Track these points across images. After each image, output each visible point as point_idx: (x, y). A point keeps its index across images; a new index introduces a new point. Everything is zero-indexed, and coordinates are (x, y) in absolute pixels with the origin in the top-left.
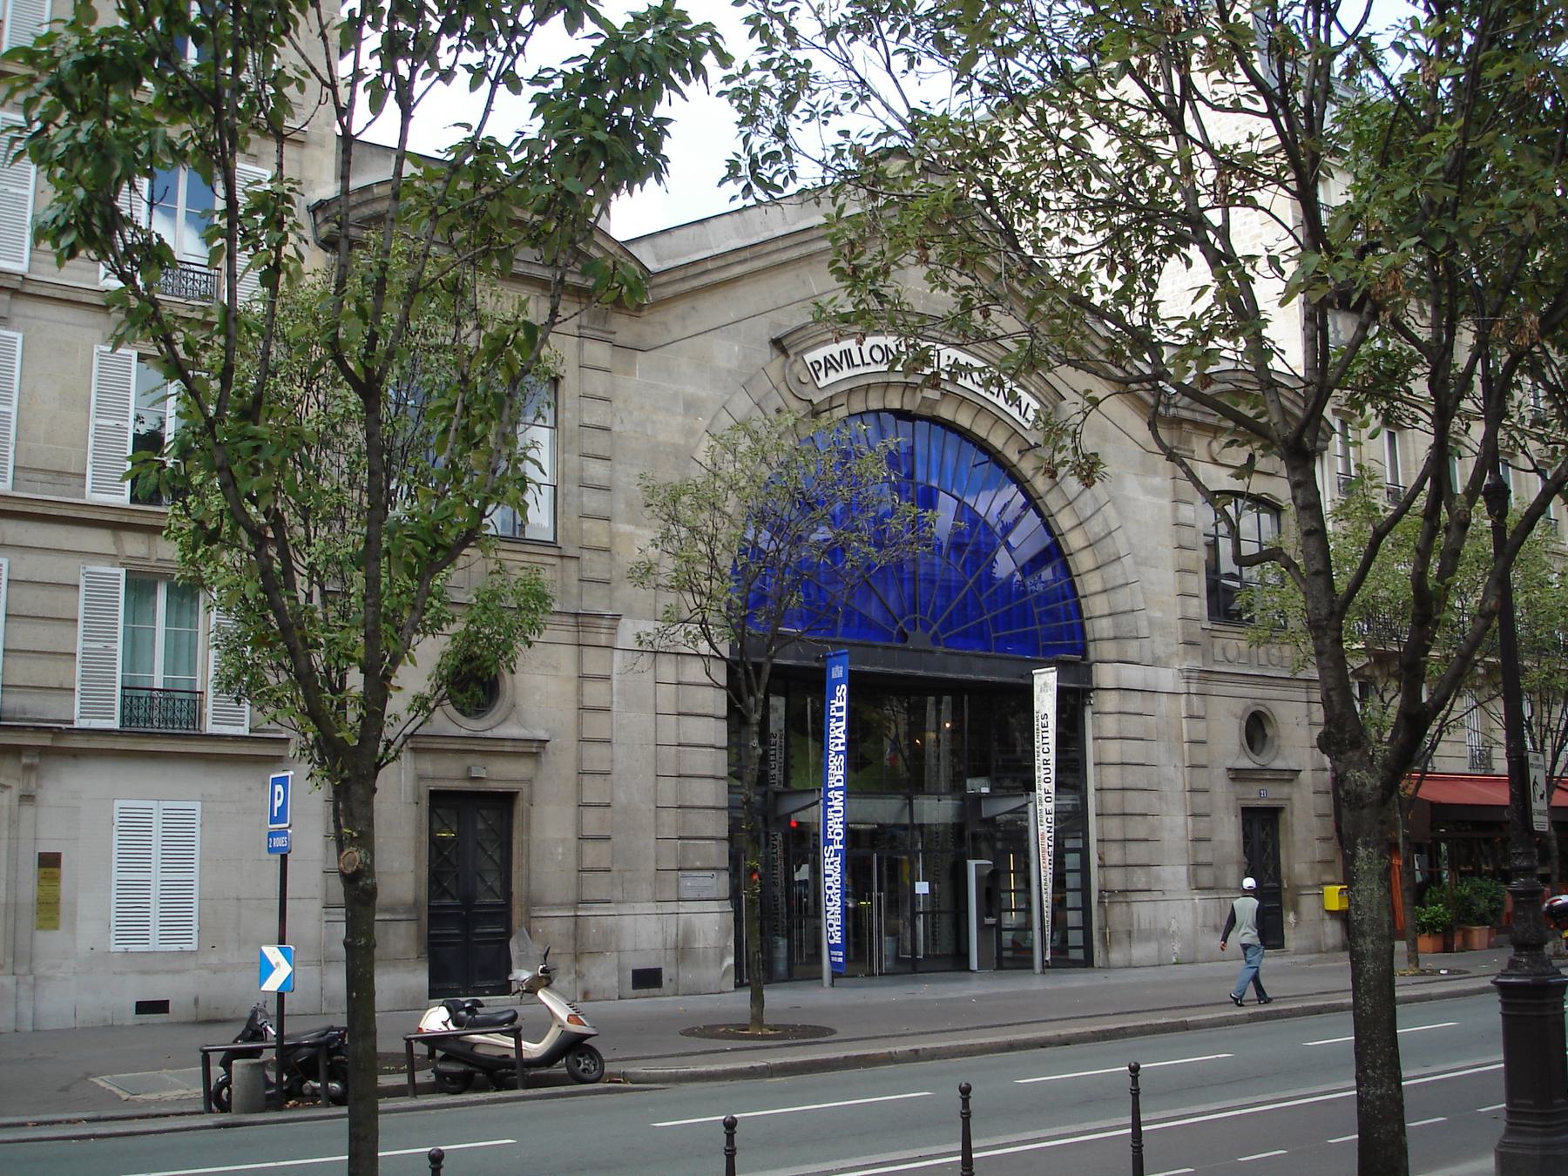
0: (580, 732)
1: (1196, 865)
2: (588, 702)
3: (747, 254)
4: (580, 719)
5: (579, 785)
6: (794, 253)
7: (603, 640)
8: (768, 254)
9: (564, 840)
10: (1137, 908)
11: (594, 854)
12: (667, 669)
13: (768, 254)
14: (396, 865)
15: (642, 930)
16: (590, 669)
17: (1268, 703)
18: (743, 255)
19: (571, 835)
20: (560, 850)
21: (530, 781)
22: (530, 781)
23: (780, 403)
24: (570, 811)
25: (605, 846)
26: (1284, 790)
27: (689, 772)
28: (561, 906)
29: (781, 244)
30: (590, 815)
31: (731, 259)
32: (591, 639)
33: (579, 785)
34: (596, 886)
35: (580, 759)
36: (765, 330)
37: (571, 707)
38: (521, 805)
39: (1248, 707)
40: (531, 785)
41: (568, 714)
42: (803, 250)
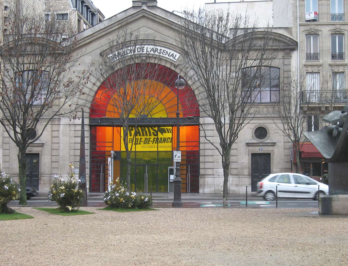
0: (52, 142)
1: (58, 131)
2: (53, 136)
3: (90, 37)
4: (52, 139)
5: (52, 152)
6: (103, 33)
7: (57, 123)
8: (96, 35)
9: (48, 162)
10: (206, 179)
11: (54, 165)
12: (73, 128)
13: (96, 35)
14: (16, 167)
15: (76, 190)
16: (54, 129)
17: (265, 125)
18: (89, 37)
19: (50, 161)
20: (48, 164)
21: (41, 151)
22: (41, 151)
23: (81, 76)
24: (50, 157)
25: (57, 163)
26: (271, 148)
27: (76, 149)
28: (48, 174)
29: (99, 33)
30: (54, 157)
31: (86, 39)
32: (54, 123)
33: (52, 152)
34: (55, 171)
35: (52, 147)
36: (98, 52)
37: (51, 137)
38: (40, 156)
39: (256, 126)
40: (42, 152)
41: (49, 138)
42: (106, 32)
